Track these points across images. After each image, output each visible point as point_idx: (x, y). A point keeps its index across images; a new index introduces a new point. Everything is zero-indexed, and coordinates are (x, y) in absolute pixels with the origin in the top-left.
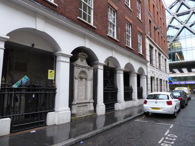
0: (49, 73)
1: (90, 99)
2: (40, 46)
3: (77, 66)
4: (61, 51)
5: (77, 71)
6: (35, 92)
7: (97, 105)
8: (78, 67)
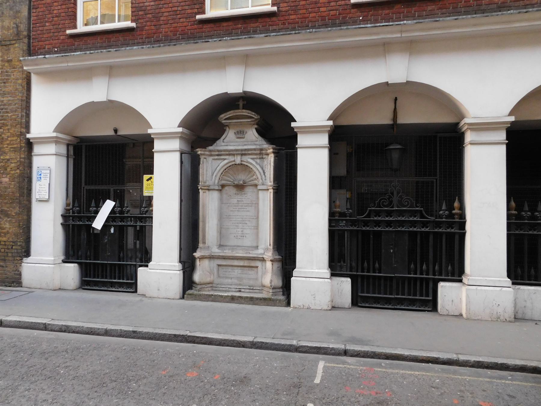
0: (145, 183)
1: (267, 249)
2: (413, 115)
3: (211, 155)
4: (151, 128)
5: (211, 169)
6: (115, 224)
7: (295, 273)
8: (218, 155)
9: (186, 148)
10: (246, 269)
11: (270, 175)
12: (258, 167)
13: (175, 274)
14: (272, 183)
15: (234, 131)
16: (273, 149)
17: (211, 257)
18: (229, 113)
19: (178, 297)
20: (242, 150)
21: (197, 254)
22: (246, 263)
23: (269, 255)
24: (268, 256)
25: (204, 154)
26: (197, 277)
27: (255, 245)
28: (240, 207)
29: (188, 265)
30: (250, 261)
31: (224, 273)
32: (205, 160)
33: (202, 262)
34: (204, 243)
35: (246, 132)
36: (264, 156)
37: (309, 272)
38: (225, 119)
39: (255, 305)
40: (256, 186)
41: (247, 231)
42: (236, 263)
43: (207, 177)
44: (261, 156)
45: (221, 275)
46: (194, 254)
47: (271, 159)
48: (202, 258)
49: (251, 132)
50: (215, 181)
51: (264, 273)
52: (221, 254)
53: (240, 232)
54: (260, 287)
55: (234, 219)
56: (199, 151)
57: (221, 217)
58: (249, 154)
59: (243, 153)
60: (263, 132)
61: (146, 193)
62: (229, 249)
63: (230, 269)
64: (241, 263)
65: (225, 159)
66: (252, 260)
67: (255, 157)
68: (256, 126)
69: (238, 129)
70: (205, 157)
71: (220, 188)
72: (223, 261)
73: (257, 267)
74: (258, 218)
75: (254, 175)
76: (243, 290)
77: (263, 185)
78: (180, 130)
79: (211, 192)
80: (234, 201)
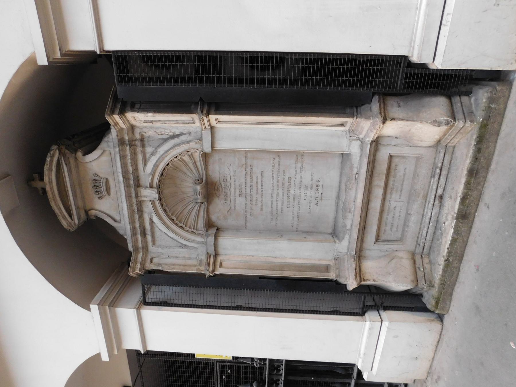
1: (352, 134)
3: (145, 248)
5: (173, 249)
8: (144, 234)
9: (136, 294)
10: (391, 183)
11: (177, 122)
12: (161, 150)
13: (389, 329)
14: (195, 116)
15: (96, 200)
16: (112, 112)
17: (359, 255)
18: (57, 211)
19: (437, 326)
20: (127, 186)
21: (352, 285)
22: (379, 182)
23: (366, 127)
24: (370, 130)
25: (143, 263)
26: (398, 284)
27: (337, 161)
28: (254, 192)
29: (373, 299)
30: (375, 174)
31: (394, 229)
32: (155, 261)
33: (367, 276)
34: (327, 268)
35: (96, 175)
36: (138, 136)
37: (428, 15)
38: (71, 216)
39: (488, 165)
40: (205, 156)
41: (307, 178)
42: (376, 204)
43: (190, 258)
44: (138, 143)
45: (399, 235)
46: (350, 288)
47: (140, 119)
48: (359, 273)
49: (94, 164)
50: (198, 243)
51: (407, 140)
52: (355, 236)
53: (308, 193)
54: (437, 152)
55: (280, 204)
56: (136, 269)
57: (277, 231)
58: (136, 169)
59: (133, 183)
60: (93, 135)
61: (231, 359)
62: (345, 217)
63: (388, 217)
64: (378, 192)
65: (152, 222)
66: (373, 168)
67: (140, 157)
68: (80, 154)
69: (91, 191)
70: (149, 260)
71: (213, 231)
72: (369, 228)
73: (391, 157)
74: (278, 153)
75: (182, 160)
76: (440, 192)
77: (201, 139)
78: (94, 307)
79: (221, 251)
80: (240, 201)
